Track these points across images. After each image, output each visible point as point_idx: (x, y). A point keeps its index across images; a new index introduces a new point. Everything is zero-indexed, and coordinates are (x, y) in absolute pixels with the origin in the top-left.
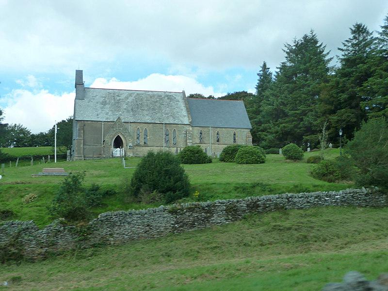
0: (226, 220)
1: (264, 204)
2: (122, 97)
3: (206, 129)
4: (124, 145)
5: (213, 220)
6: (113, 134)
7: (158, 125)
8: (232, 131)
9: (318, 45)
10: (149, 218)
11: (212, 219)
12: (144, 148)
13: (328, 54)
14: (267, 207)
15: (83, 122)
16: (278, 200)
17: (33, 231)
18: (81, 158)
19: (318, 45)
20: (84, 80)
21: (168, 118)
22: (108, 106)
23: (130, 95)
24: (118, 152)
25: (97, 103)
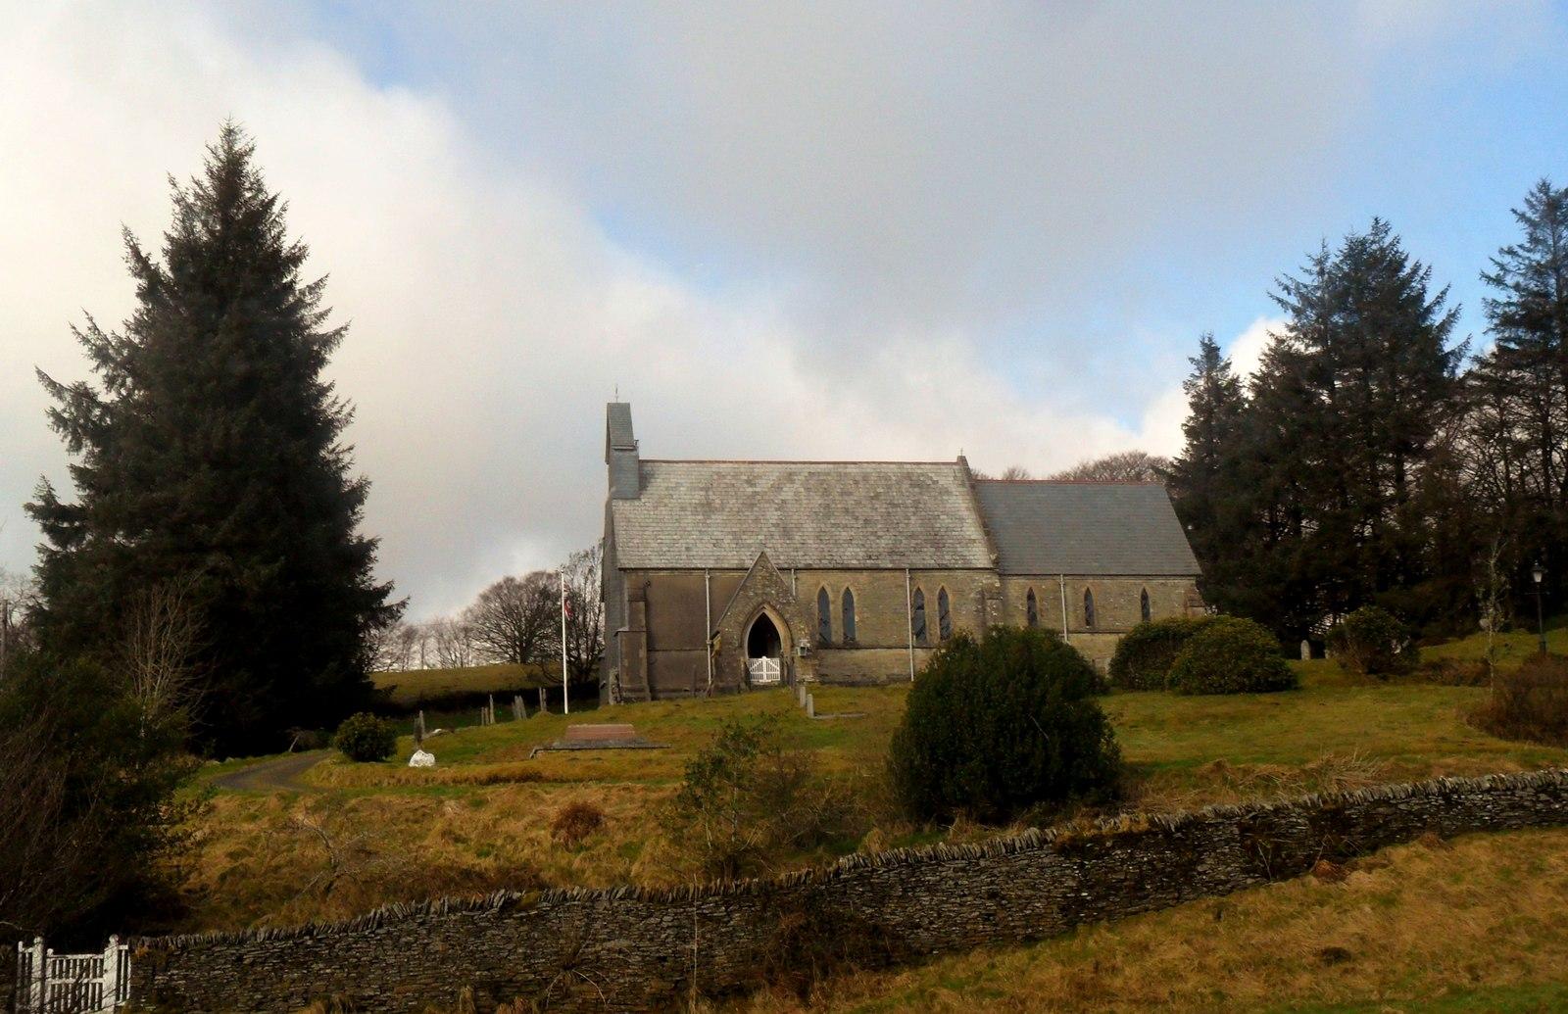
0: (1245, 871)
1: (1369, 817)
2: (763, 485)
3: (1047, 584)
4: (785, 644)
5: (1204, 873)
6: (749, 609)
7: (886, 574)
8: (1136, 587)
9: (1407, 270)
10: (995, 872)
11: (1200, 869)
12: (846, 654)
13: (1439, 300)
14: (1379, 827)
15: (641, 573)
16: (1414, 800)
17: (632, 919)
18: (641, 695)
19: (1407, 270)
20: (635, 438)
21: (917, 550)
22: (717, 518)
23: (790, 477)
24: (767, 669)
25: (683, 509)
